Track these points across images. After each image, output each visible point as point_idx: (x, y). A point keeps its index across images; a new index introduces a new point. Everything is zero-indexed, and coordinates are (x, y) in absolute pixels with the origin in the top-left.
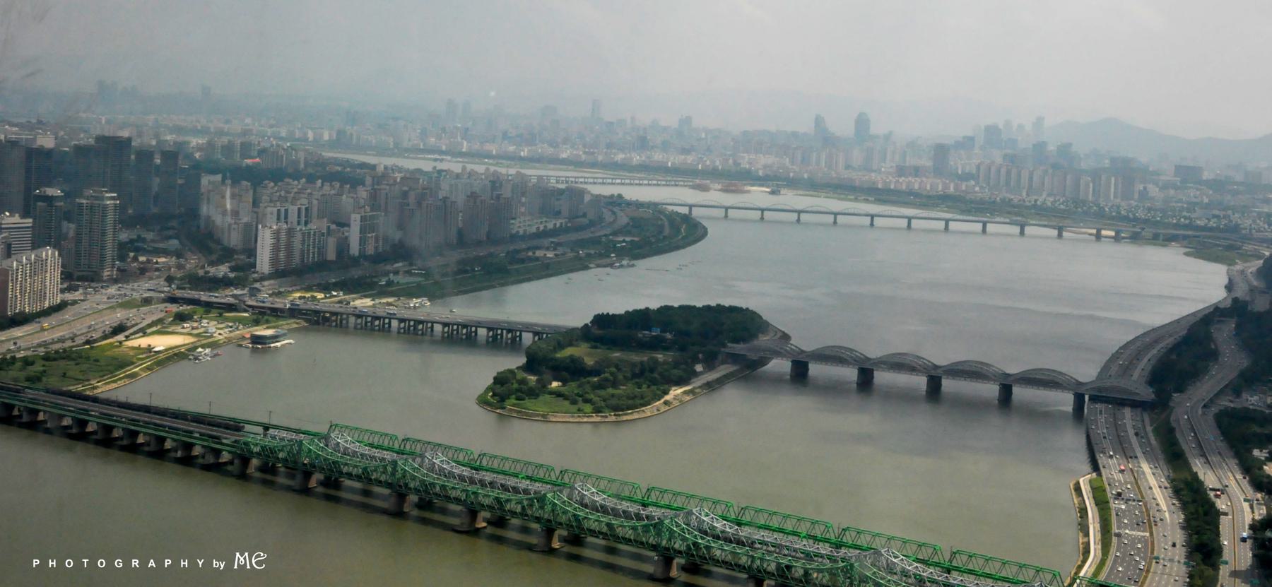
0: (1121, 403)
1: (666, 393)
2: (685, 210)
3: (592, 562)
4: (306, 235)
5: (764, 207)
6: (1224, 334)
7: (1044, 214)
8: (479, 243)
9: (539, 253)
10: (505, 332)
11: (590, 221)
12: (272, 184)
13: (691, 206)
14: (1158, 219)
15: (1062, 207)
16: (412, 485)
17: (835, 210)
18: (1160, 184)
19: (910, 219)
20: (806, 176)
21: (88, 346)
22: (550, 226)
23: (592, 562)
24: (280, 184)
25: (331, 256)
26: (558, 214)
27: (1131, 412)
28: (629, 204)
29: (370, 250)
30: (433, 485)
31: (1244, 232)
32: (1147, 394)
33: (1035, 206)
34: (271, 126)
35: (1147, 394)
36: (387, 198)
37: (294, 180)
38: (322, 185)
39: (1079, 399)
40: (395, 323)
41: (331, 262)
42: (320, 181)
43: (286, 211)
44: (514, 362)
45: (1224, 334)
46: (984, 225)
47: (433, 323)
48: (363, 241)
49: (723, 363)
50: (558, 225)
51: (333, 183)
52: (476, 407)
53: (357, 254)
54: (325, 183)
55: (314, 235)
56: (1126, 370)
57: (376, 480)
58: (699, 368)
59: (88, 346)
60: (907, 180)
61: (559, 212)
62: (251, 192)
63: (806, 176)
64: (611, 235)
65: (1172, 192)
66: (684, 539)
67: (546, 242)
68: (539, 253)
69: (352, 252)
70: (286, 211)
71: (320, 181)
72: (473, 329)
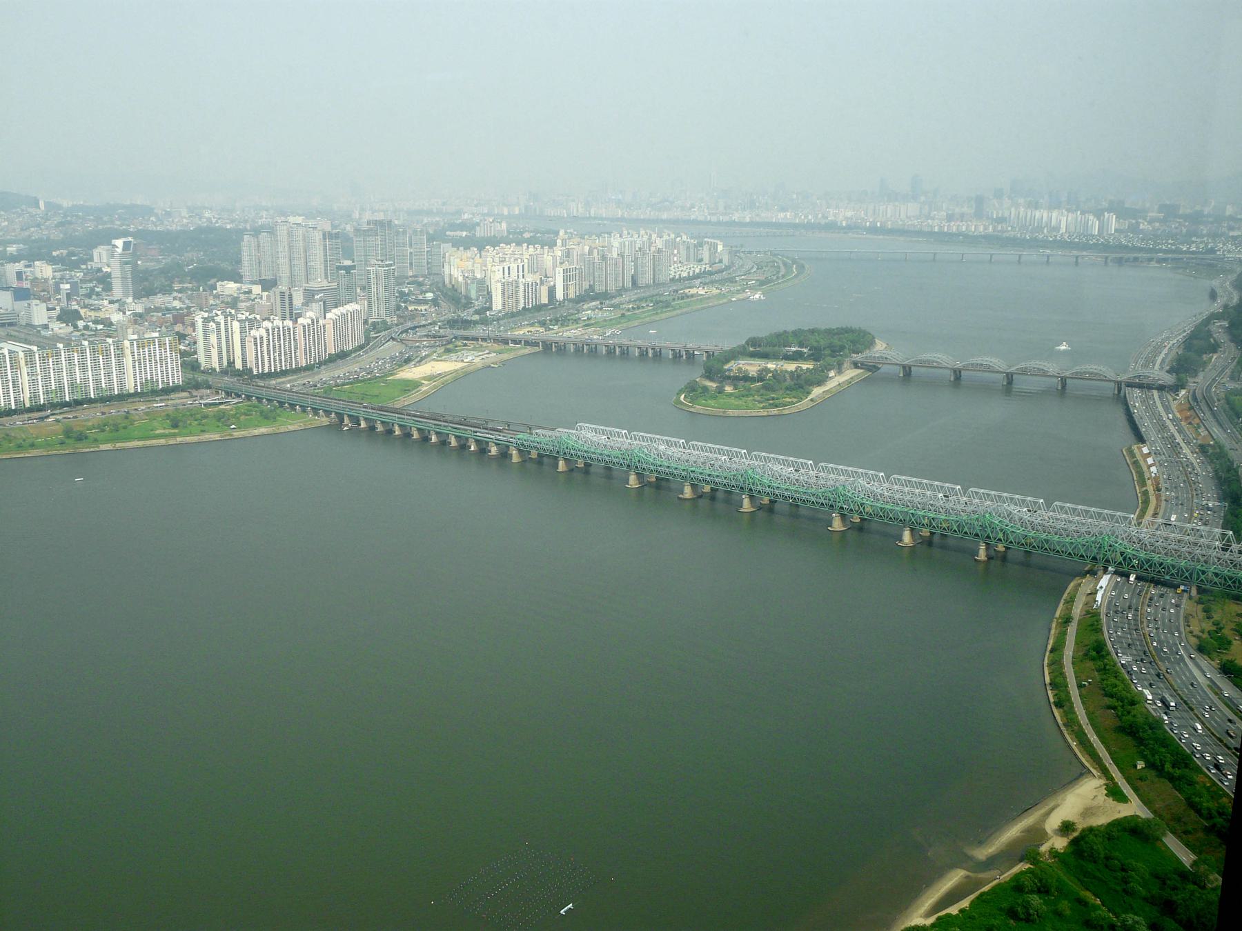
1: (809, 393)
4: (527, 285)
6: (1219, 330)
8: (647, 286)
11: (726, 266)
12: (492, 248)
14: (1151, 246)
15: (1076, 240)
18: (1148, 219)
21: (850, 374)
24: (497, 248)
25: (545, 300)
27: (1158, 392)
29: (572, 296)
31: (1218, 253)
32: (1169, 379)
33: (1055, 241)
34: (476, 206)
35: (1169, 379)
37: (507, 245)
38: (528, 247)
41: (545, 305)
42: (526, 244)
43: (509, 268)
48: (566, 288)
51: (536, 246)
53: (562, 299)
54: (530, 246)
55: (532, 285)
58: (832, 374)
59: (850, 374)
60: (956, 224)
62: (479, 254)
64: (475, 323)
65: (1157, 225)
67: (698, 282)
68: (693, 291)
69: (237, 367)
70: (509, 268)
71: (526, 244)
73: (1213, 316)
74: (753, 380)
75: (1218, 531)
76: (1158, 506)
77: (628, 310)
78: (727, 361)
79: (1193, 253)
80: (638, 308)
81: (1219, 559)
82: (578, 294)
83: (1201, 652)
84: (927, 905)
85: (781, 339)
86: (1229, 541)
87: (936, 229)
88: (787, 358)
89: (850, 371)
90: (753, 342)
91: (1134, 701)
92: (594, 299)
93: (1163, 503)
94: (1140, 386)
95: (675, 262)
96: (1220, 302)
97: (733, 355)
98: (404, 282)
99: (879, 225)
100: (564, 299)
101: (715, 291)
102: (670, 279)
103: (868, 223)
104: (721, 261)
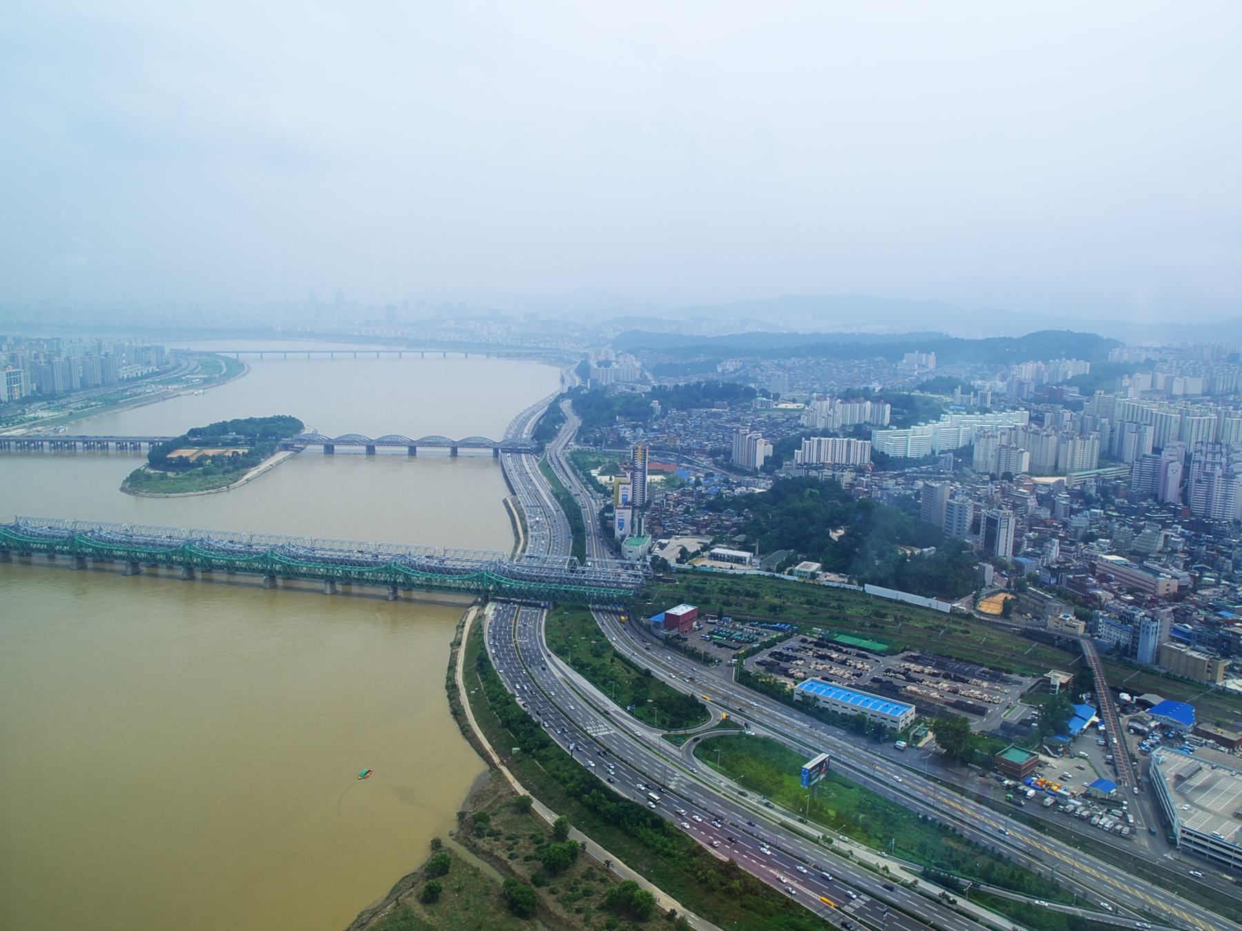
0: (519, 452)
2: (234, 356)
3: (163, 577)
5: (286, 350)
6: (566, 405)
7: (456, 346)
8: (97, 386)
9: (140, 390)
10: (128, 444)
13: (237, 353)
16: (12, 545)
17: (378, 350)
19: (378, 352)
20: (309, 329)
22: (145, 372)
23: (163, 577)
26: (149, 363)
28: (196, 353)
30: (102, 549)
36: (23, 360)
39: (496, 451)
40: (46, 444)
44: (141, 464)
45: (566, 405)
46: (423, 353)
47: (42, 441)
49: (280, 450)
50: (150, 371)
52: (129, 499)
56: (520, 430)
57: (59, 550)
61: (150, 362)
63: (309, 329)
66: (199, 556)
72: (40, 443)
73: (562, 396)
74: (193, 466)
75: (569, 558)
76: (526, 543)
77: (77, 409)
78: (170, 451)
79: (548, 349)
80: (87, 407)
81: (568, 579)
82: (24, 395)
83: (562, 655)
84: (617, 790)
85: (223, 428)
86: (575, 564)
87: (356, 333)
88: (225, 445)
89: (282, 453)
90: (193, 432)
91: (509, 701)
92: (40, 399)
93: (530, 539)
94: (511, 451)
95: (124, 365)
96: (567, 384)
97: (182, 442)
98: (948, 504)
99: (300, 329)
100: (9, 401)
101: (135, 390)
102: (119, 380)
103: (300, 329)
104: (168, 363)
